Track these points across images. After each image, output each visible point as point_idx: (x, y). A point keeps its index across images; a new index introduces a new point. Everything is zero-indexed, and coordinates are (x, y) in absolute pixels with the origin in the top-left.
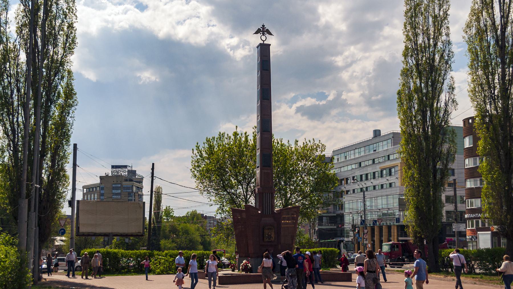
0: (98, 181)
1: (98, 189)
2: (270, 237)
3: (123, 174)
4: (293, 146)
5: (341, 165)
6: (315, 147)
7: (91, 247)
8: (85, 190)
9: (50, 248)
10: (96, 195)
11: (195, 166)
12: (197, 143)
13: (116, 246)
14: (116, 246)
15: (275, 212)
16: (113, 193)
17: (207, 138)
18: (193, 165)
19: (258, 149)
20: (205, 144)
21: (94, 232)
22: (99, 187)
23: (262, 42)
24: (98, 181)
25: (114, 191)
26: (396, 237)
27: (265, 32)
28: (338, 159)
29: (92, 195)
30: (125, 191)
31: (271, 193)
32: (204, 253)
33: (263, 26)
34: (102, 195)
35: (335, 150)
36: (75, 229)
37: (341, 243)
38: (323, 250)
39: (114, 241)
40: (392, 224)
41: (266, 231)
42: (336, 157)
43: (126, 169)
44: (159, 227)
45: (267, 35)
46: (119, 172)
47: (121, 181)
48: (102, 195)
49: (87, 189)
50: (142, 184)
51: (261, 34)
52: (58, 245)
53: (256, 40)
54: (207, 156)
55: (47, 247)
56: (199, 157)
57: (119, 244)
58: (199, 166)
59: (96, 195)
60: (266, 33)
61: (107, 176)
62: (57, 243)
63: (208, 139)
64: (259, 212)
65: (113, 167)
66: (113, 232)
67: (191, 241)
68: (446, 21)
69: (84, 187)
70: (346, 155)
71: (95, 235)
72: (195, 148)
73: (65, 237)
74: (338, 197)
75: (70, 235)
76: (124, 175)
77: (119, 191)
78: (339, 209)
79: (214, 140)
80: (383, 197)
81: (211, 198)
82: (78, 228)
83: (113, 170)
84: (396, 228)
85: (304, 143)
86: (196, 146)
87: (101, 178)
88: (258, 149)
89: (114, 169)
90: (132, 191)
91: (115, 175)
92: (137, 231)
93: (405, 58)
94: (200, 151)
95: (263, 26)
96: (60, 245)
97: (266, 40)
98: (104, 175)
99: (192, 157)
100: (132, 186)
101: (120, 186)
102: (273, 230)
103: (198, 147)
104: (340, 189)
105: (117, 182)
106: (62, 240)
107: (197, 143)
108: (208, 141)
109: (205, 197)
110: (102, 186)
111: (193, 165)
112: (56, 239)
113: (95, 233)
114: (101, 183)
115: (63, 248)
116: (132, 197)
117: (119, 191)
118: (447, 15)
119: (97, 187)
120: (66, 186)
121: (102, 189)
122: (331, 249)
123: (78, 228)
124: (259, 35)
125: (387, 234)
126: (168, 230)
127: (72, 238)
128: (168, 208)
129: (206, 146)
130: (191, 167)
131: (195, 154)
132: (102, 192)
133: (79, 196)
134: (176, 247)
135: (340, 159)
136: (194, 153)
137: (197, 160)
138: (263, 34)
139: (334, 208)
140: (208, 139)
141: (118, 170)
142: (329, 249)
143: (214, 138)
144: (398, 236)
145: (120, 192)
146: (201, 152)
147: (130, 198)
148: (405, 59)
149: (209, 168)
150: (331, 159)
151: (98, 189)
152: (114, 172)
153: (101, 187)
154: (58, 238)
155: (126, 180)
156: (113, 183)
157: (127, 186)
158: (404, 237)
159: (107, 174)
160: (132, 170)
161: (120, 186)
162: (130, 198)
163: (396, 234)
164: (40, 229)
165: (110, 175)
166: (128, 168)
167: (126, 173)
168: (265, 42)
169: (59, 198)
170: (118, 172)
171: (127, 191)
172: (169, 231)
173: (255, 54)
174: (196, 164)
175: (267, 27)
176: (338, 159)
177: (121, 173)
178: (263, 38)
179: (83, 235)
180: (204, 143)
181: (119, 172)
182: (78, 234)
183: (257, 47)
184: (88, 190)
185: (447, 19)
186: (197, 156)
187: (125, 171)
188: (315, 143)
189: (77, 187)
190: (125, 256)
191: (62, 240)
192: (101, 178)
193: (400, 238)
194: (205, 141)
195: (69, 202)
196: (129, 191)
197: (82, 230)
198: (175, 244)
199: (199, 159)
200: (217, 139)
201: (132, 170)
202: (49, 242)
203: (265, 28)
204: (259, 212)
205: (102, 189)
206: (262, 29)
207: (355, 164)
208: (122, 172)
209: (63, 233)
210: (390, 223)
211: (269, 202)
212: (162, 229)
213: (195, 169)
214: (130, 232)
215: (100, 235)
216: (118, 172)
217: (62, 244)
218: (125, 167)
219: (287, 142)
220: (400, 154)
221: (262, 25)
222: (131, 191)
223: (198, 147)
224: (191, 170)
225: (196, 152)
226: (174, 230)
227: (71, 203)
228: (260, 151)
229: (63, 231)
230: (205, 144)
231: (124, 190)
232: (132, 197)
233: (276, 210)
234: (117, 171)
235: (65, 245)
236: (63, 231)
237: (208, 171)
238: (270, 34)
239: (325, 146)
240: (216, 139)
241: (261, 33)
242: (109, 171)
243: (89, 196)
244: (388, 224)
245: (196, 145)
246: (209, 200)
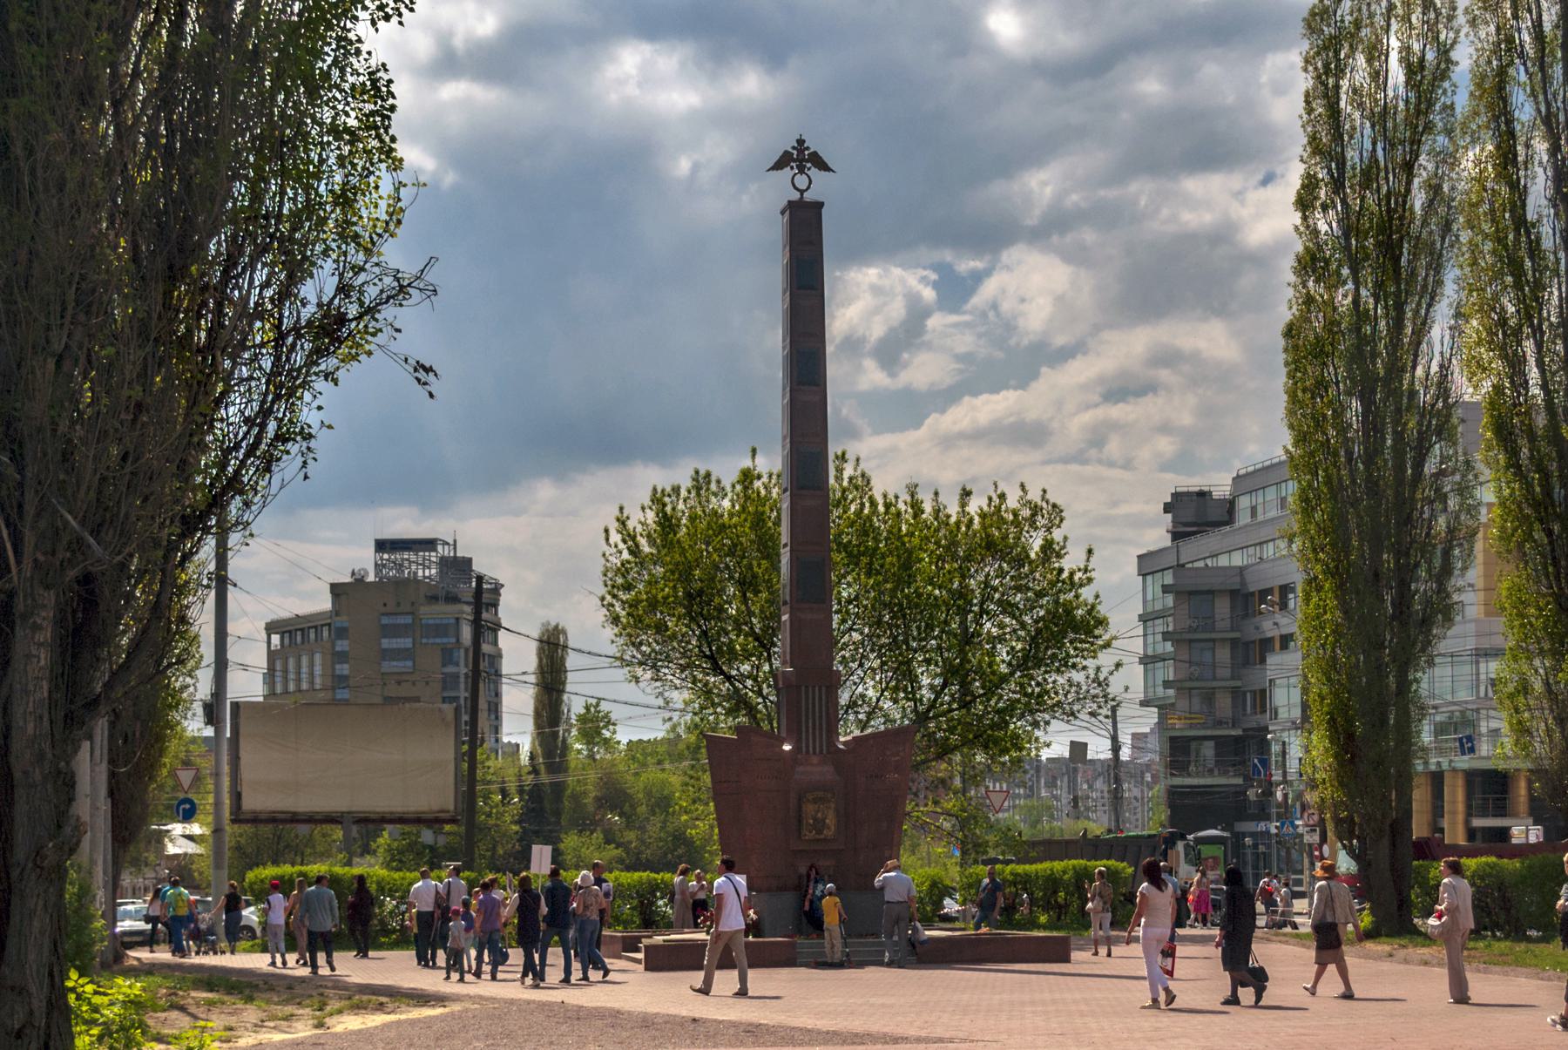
0: (324, 603)
1: (326, 633)
2: (819, 825)
3: (420, 573)
4: (953, 510)
5: (1265, 533)
6: (1026, 513)
7: (299, 860)
8: (276, 639)
9: (146, 865)
10: (318, 658)
11: (613, 587)
12: (621, 509)
13: (392, 860)
14: (392, 860)
15: (841, 747)
16: (385, 651)
17: (655, 489)
18: (609, 583)
19: (785, 545)
20: (648, 511)
21: (292, 809)
22: (329, 625)
23: (796, 196)
24: (324, 603)
25: (386, 643)
26: (1460, 818)
27: (807, 161)
28: (1254, 510)
29: (305, 660)
30: (431, 641)
31: (827, 687)
32: (656, 879)
33: (801, 142)
34: (341, 657)
35: (1242, 472)
36: (227, 801)
37: (1174, 844)
38: (1074, 868)
39: (384, 839)
40: (1445, 766)
41: (809, 809)
42: (1244, 503)
43: (433, 554)
44: (558, 788)
45: (814, 172)
46: (406, 564)
47: (413, 604)
48: (341, 657)
49: (282, 634)
50: (496, 613)
51: (792, 168)
52: (176, 856)
53: (781, 188)
54: (654, 551)
55: (138, 863)
56: (626, 555)
57: (401, 852)
58: (628, 587)
59: (318, 658)
60: (809, 165)
61: (359, 581)
62: (171, 849)
63: (659, 490)
64: (787, 747)
65: (381, 545)
66: (354, 809)
67: (680, 838)
68: (1446, 84)
69: (271, 628)
70: (1284, 494)
71: (312, 819)
72: (613, 526)
73: (202, 824)
74: (1247, 663)
75: (210, 819)
76: (425, 577)
77: (406, 643)
78: (1254, 706)
79: (679, 495)
80: (1193, 692)
81: (666, 694)
82: (237, 797)
83: (382, 559)
84: (1460, 782)
85: (990, 499)
86: (618, 520)
87: (337, 590)
88: (785, 545)
89: (386, 556)
90: (458, 640)
91: (389, 579)
92: (436, 807)
93: (1304, 214)
94: (629, 535)
95: (801, 142)
96: (186, 854)
97: (808, 188)
98: (348, 579)
99: (604, 555)
100: (457, 619)
101: (408, 620)
102: (833, 805)
103: (622, 522)
104: (1257, 628)
105: (398, 604)
106: (190, 838)
107: (621, 509)
108: (657, 499)
109: (648, 690)
110: (342, 621)
111: (609, 583)
112: (168, 831)
113: (295, 814)
114: (336, 611)
115: (194, 867)
116: (457, 664)
117: (406, 643)
118: (1449, 61)
119: (322, 625)
120: (191, 670)
121: (342, 633)
122: (1046, 865)
123: (237, 797)
124: (787, 173)
125: (1427, 807)
126: (592, 795)
127: (218, 831)
128: (592, 709)
129: (651, 516)
130: (603, 591)
131: (616, 546)
132: (342, 645)
133: (247, 685)
134: (621, 861)
135: (1260, 510)
136: (612, 541)
137: (623, 565)
138: (801, 170)
139: (1234, 706)
140: (659, 490)
141: (403, 559)
142: (1040, 867)
143: (676, 490)
144: (1469, 814)
145: (411, 646)
146: (633, 538)
147: (450, 669)
148: (1305, 218)
149: (655, 597)
150: (1230, 506)
151: (326, 633)
152: (384, 566)
153: (338, 625)
154: (177, 828)
155: (434, 599)
156: (384, 610)
157: (438, 621)
158: (1495, 816)
159: (358, 577)
160: (455, 557)
161: (408, 620)
162: (450, 669)
163: (1461, 807)
164: (114, 805)
165: (371, 578)
166: (440, 548)
167: (433, 571)
168: (808, 196)
169: (170, 707)
170: (399, 567)
171: (438, 640)
172: (597, 799)
173: (777, 230)
174: (620, 581)
175: (813, 145)
176: (1254, 510)
177: (414, 568)
178: (801, 181)
179: (256, 819)
180: (643, 509)
181: (406, 564)
182: (238, 817)
183: (783, 213)
184: (287, 641)
185: (1450, 78)
186: (621, 552)
187: (427, 563)
188: (1029, 497)
189: (230, 656)
190: (390, 890)
191: (190, 838)
192: (337, 590)
193: (1478, 822)
194: (647, 502)
195: (204, 709)
196: (445, 640)
197: (250, 803)
198: (617, 848)
199: (628, 562)
200: (689, 492)
201: (455, 557)
202: (142, 845)
203: (808, 148)
204: (787, 747)
205: (342, 633)
206: (795, 152)
207: (1255, 545)
208: (418, 564)
209: (188, 816)
210: (1439, 763)
211: (821, 717)
212: (569, 792)
213: (614, 596)
214: (412, 809)
215: (331, 819)
216: (401, 565)
217: (190, 851)
218: (430, 544)
219: (932, 496)
220: (1291, 541)
221: (798, 141)
222: (453, 640)
223: (622, 522)
224: (603, 599)
225: (615, 538)
226: (614, 796)
227: (212, 713)
228: (791, 551)
229: (187, 806)
230: (648, 511)
231: (427, 637)
232: (457, 664)
233: (842, 739)
234: (399, 561)
235: (202, 855)
236: (187, 806)
237: (653, 605)
238: (823, 166)
239: (1062, 511)
240: (684, 493)
241: (794, 164)
242: (364, 559)
243: (291, 663)
244: (1433, 768)
245: (617, 513)
246: (660, 702)
